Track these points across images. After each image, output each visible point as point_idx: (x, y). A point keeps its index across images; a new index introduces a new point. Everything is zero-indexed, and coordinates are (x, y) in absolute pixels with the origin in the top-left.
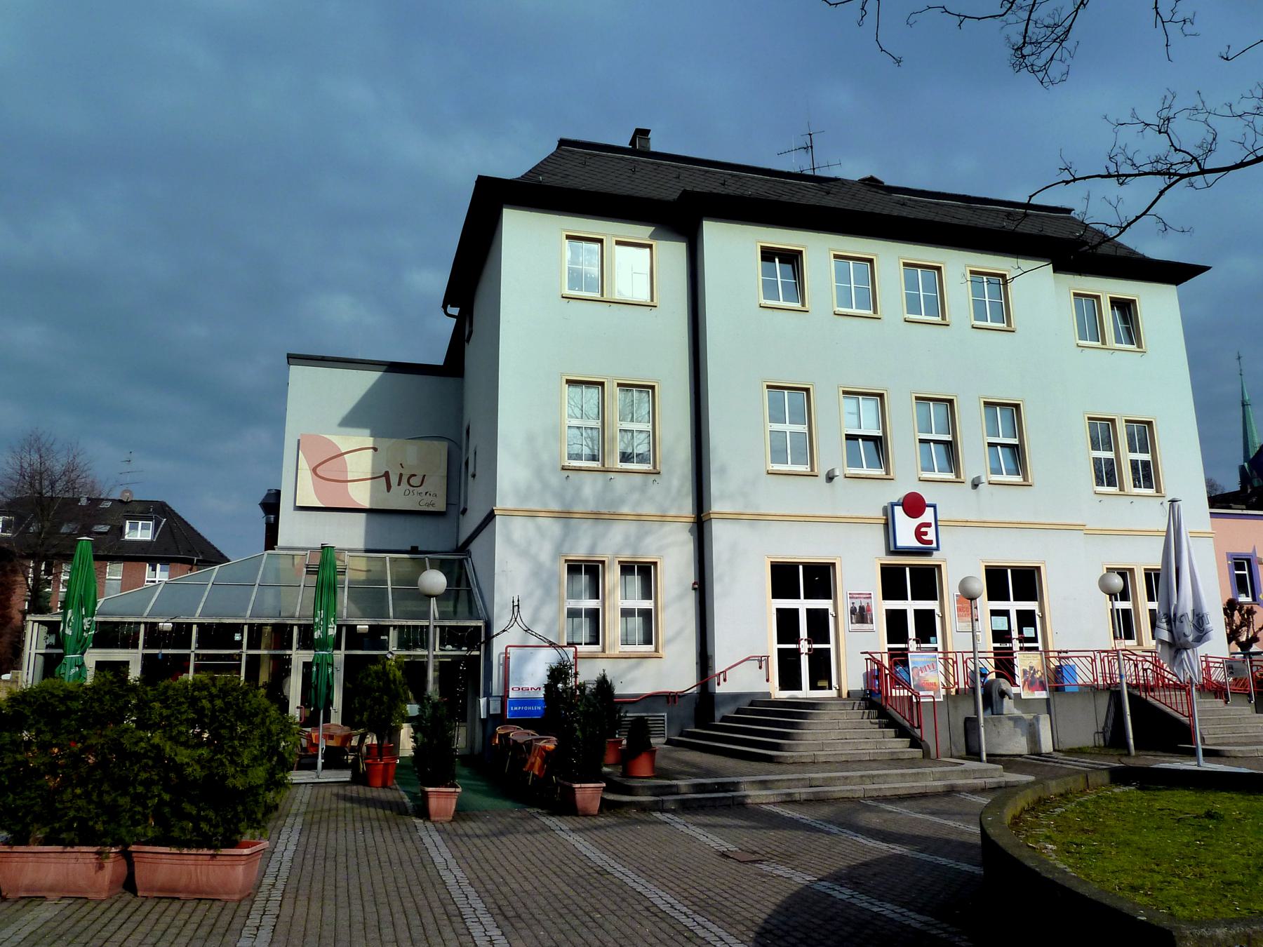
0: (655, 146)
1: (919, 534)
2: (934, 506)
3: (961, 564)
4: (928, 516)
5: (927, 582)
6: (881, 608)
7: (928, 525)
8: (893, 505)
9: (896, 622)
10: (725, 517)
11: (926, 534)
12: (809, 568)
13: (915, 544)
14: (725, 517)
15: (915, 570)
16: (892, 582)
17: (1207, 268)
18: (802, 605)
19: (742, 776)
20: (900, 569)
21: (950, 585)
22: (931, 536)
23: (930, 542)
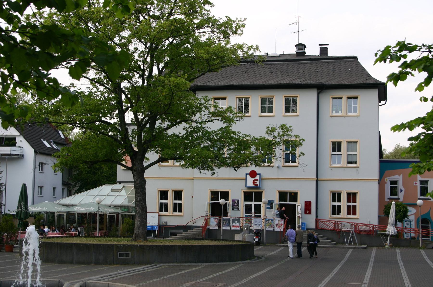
0: (330, 54)
1: (254, 182)
2: (260, 174)
3: (270, 194)
4: (258, 177)
5: (259, 196)
6: (243, 204)
7: (257, 180)
8: (246, 174)
9: (248, 209)
10: (131, 182)
11: (256, 182)
12: (290, 193)
13: (253, 185)
14: (131, 182)
15: (255, 193)
16: (248, 196)
17: (374, 65)
18: (253, 203)
19: (271, 269)
20: (251, 193)
21: (265, 199)
22: (258, 183)
23: (257, 185)
